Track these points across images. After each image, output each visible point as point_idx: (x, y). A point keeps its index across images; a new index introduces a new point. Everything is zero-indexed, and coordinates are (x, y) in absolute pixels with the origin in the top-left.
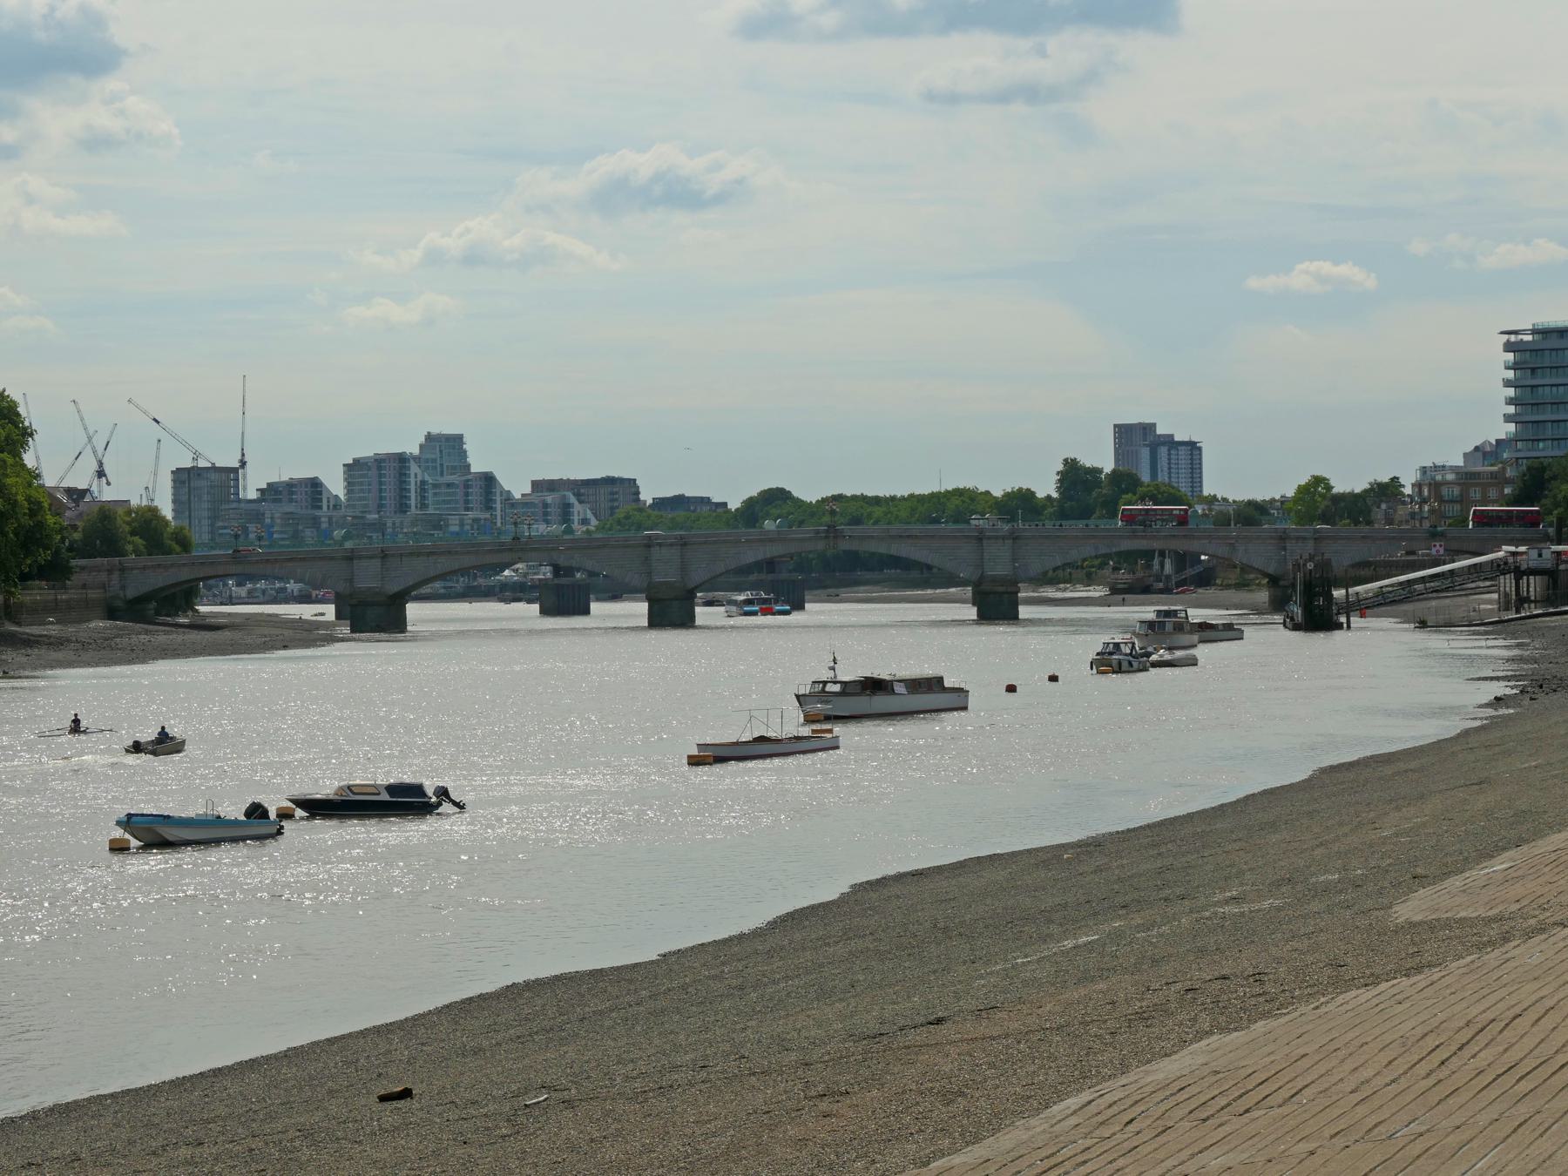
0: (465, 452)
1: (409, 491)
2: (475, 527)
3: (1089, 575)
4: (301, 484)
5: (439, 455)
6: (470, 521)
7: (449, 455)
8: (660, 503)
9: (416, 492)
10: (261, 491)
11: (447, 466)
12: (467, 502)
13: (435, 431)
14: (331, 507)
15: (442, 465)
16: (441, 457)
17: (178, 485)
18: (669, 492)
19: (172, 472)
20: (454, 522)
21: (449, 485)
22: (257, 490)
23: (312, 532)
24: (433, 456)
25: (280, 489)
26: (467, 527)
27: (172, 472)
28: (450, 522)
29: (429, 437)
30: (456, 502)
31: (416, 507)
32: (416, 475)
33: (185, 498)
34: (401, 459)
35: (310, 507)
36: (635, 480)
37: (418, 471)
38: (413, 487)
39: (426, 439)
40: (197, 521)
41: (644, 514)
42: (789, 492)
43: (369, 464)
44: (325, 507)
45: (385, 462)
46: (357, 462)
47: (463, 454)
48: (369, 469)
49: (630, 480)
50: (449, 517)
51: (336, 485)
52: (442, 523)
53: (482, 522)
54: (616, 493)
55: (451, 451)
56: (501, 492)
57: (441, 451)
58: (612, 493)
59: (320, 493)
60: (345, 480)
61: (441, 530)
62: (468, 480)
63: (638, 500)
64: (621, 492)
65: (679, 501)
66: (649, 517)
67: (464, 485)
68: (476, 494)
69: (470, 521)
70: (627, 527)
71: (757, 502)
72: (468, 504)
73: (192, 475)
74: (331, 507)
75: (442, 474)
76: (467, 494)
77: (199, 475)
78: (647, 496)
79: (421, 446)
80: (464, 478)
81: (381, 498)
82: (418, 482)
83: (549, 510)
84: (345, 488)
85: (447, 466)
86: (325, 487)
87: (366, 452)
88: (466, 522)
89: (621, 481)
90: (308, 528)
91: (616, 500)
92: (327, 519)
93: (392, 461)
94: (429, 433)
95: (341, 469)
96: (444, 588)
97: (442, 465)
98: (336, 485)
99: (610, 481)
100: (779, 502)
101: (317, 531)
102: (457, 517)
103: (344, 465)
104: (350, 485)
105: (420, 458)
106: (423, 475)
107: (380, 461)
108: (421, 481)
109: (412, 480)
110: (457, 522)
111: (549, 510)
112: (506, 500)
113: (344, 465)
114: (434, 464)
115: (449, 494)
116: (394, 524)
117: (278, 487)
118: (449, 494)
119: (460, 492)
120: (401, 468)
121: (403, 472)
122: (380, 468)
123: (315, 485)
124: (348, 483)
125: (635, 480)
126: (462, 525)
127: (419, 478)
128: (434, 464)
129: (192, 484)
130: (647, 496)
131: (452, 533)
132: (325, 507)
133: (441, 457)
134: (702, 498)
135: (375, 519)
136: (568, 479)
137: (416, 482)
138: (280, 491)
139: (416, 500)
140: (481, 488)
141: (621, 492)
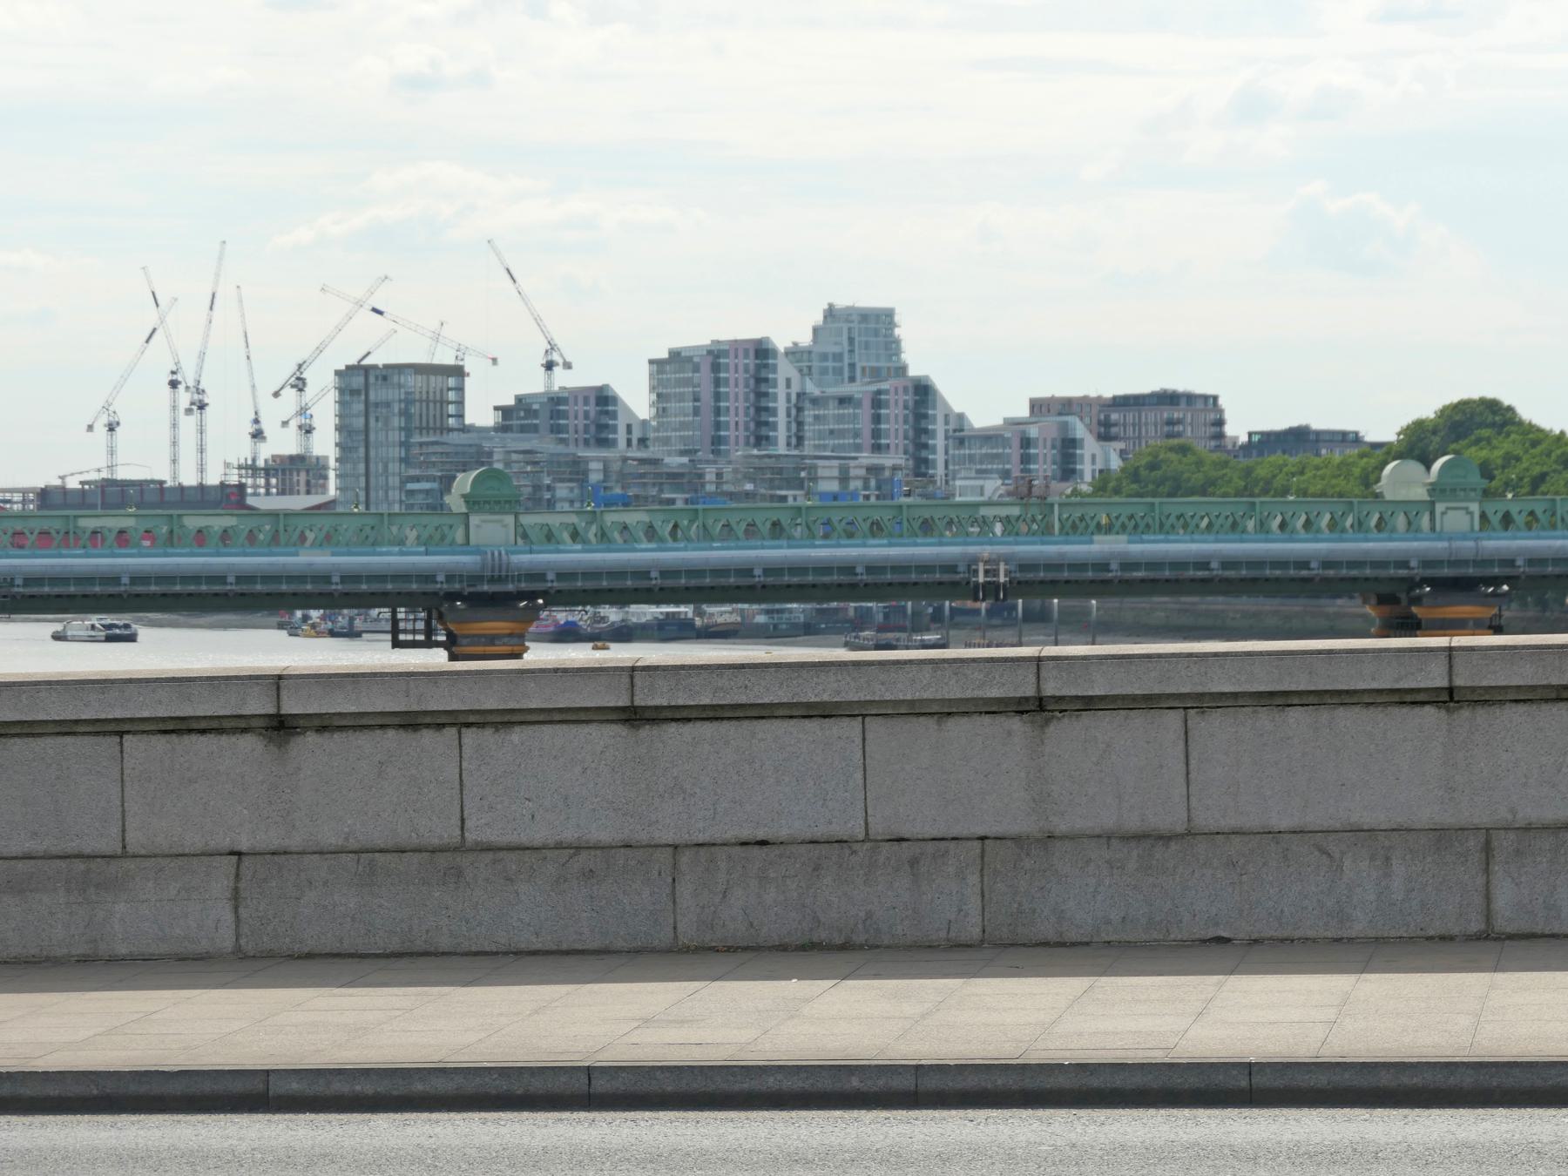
0: (897, 342)
1: (774, 412)
2: (873, 483)
3: (354, 392)
4: (576, 398)
5: (846, 347)
6: (862, 472)
7: (867, 348)
8: (1267, 442)
9: (789, 415)
10: (505, 411)
11: (863, 369)
12: (876, 434)
13: (842, 302)
14: (635, 442)
15: (852, 366)
16: (851, 351)
17: (348, 398)
18: (1279, 422)
19: (338, 373)
20: (826, 473)
21: (843, 401)
22: (496, 408)
23: (571, 489)
24: (837, 349)
25: (536, 407)
26: (855, 485)
27: (338, 373)
28: (820, 473)
29: (831, 313)
30: (857, 434)
31: (789, 444)
32: (788, 382)
33: (359, 422)
34: (762, 351)
35: (592, 441)
36: (1215, 398)
37: (794, 374)
38: (781, 405)
39: (825, 317)
40: (380, 466)
41: (1190, 458)
42: (1510, 409)
43: (696, 360)
44: (622, 443)
45: (727, 356)
46: (676, 356)
47: (892, 346)
48: (696, 369)
49: (1205, 398)
50: (820, 463)
51: (638, 400)
52: (803, 474)
53: (887, 474)
54: (1179, 422)
55: (872, 339)
56: (946, 416)
57: (851, 340)
58: (1170, 422)
59: (614, 415)
60: (652, 389)
61: (801, 487)
62: (879, 392)
63: (1220, 436)
64: (1189, 419)
65: (1299, 438)
66: (1199, 463)
67: (873, 400)
68: (896, 424)
69: (862, 472)
70: (1151, 487)
71: (1434, 432)
72: (1028, 462)
73: (372, 380)
74: (635, 442)
75: (852, 379)
76: (877, 419)
77: (385, 378)
78: (1238, 429)
79: (816, 330)
80: (874, 388)
81: (718, 426)
82: (794, 397)
83: (1032, 451)
84: (652, 405)
85: (863, 369)
86: (623, 402)
87: (697, 334)
88: (853, 473)
89: (1190, 398)
90: (562, 481)
91: (1179, 435)
92: (600, 466)
93: (741, 354)
94: (831, 306)
95: (645, 370)
96: (768, 612)
97: (852, 366)
98: (638, 400)
99: (1168, 399)
100: (1485, 432)
101: (582, 487)
102: (835, 463)
103: (651, 362)
104: (661, 398)
105: (810, 352)
106: (803, 384)
107: (717, 356)
108: (799, 395)
109: (781, 391)
110: (836, 473)
111: (1032, 451)
112: (955, 431)
113: (651, 362)
114: (837, 364)
115: (840, 419)
116: (719, 475)
117: (531, 404)
118: (840, 419)
119: (865, 412)
120: (759, 368)
121: (763, 375)
122: (716, 368)
123: (603, 399)
124: (659, 395)
125: (1215, 398)
126: (844, 478)
127: (795, 389)
128: (837, 364)
129: (372, 397)
130: (1238, 429)
131: (823, 496)
132: (622, 443)
133: (851, 351)
134: (1344, 434)
135: (683, 465)
136: (1099, 398)
137: (788, 395)
138: (536, 411)
139: (789, 429)
140: (906, 407)
141: (1189, 419)
